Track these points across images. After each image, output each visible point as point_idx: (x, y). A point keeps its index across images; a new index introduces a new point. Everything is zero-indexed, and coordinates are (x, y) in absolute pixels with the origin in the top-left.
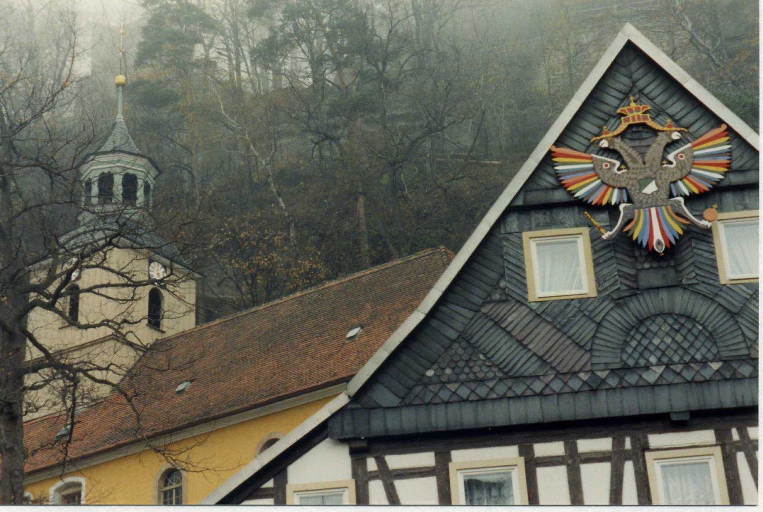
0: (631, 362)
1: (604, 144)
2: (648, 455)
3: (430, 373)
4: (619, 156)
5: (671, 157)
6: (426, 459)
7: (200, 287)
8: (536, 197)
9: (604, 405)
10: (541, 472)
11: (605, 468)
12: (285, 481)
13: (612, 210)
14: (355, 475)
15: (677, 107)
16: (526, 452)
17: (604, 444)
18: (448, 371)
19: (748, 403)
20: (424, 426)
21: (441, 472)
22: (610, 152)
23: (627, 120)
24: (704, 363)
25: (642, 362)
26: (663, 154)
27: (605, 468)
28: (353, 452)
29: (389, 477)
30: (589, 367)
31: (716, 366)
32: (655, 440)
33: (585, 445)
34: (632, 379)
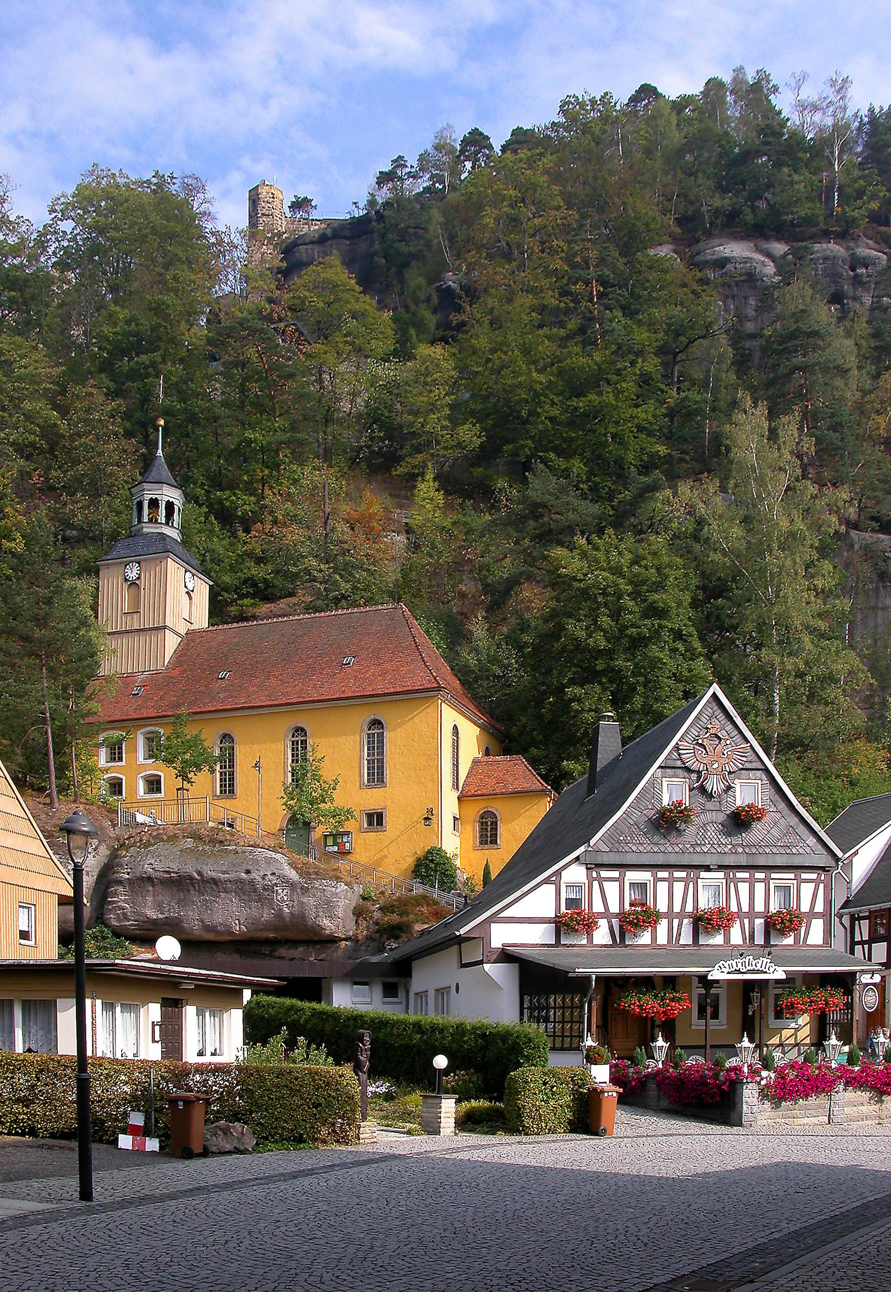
3: (621, 838)
4: (705, 749)
6: (615, 874)
7: (328, 1027)
8: (670, 763)
13: (699, 773)
15: (729, 727)
17: (683, 874)
19: (61, 907)
21: (621, 880)
28: (587, 869)
29: (601, 880)
31: (730, 847)
32: (773, 876)
33: (677, 874)
34: (698, 849)
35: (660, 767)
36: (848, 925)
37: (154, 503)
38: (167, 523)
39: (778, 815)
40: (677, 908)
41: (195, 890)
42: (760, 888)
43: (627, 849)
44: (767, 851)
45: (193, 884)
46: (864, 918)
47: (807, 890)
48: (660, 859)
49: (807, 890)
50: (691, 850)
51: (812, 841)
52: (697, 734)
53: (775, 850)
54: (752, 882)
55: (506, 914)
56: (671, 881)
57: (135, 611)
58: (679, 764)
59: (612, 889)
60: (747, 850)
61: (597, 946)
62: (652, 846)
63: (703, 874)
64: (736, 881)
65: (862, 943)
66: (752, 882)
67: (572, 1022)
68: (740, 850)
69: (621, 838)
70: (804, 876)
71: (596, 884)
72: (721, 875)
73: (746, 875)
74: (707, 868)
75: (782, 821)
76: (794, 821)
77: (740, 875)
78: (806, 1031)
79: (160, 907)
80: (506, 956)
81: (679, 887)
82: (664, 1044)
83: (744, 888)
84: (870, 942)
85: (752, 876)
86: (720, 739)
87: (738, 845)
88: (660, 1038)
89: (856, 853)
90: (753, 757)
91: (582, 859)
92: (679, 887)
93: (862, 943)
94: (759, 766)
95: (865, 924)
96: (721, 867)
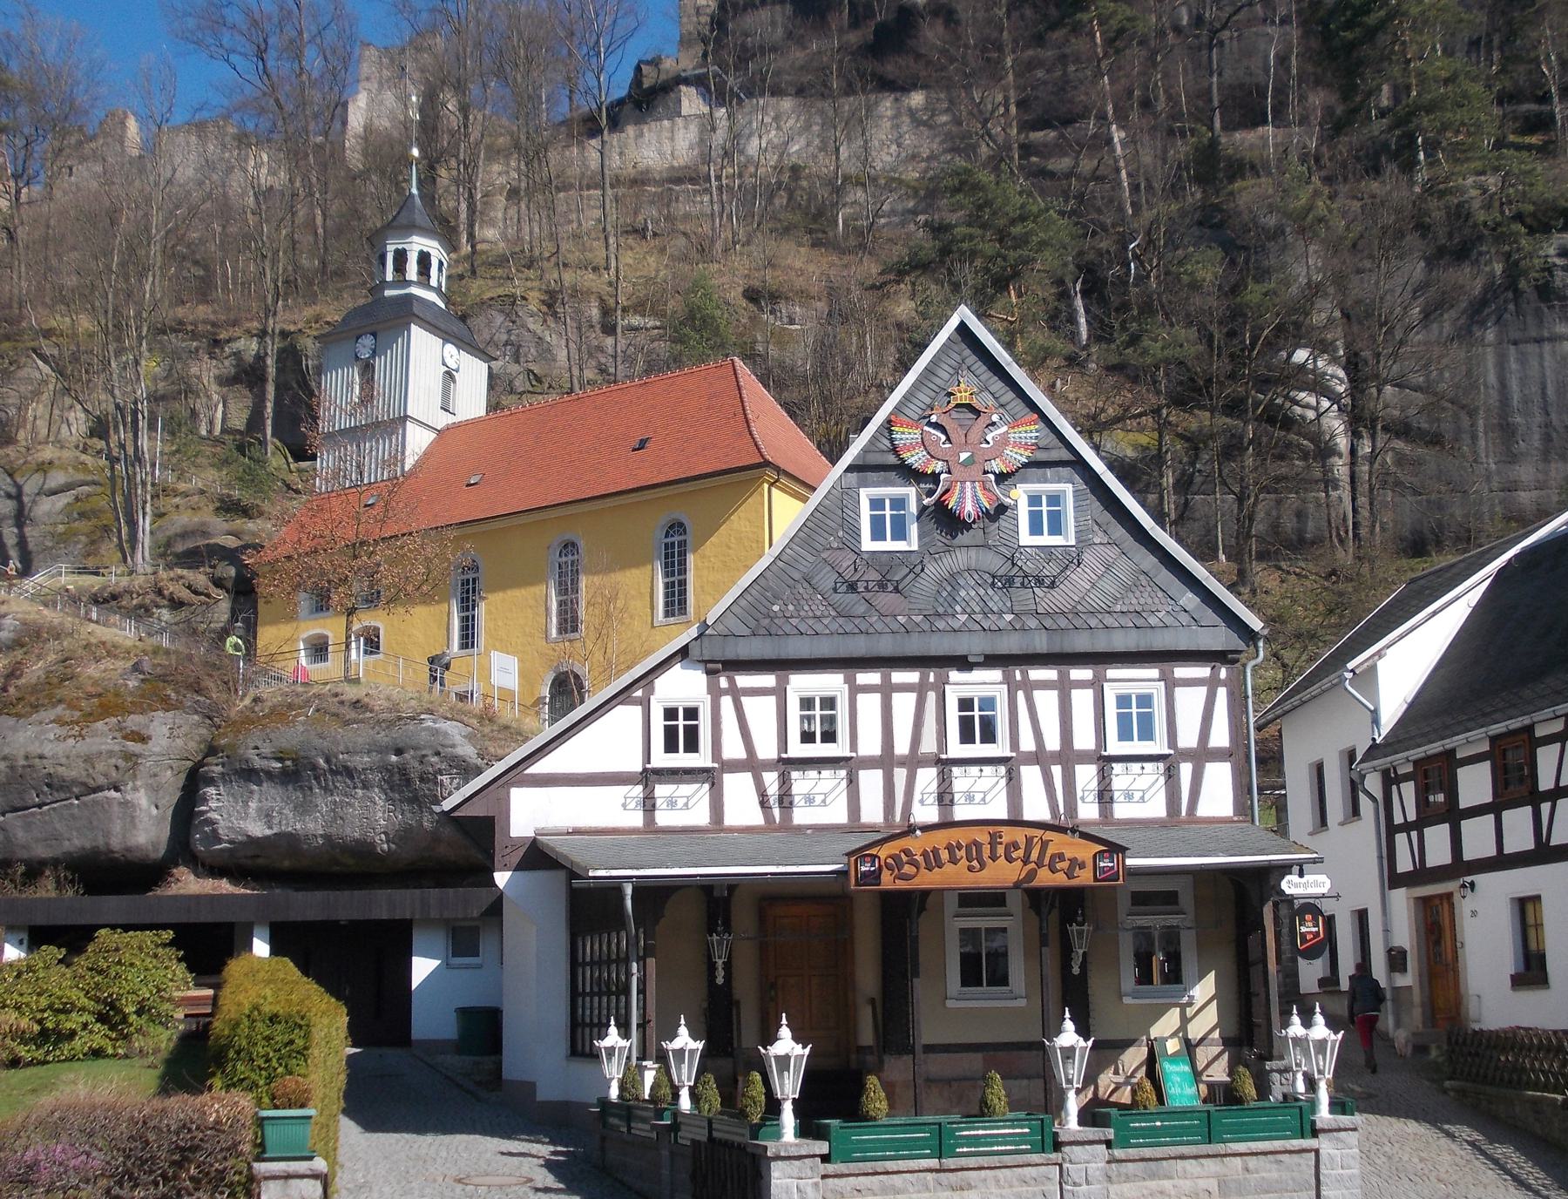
0: (941, 610)
1: (934, 419)
2: (947, 687)
3: (776, 608)
5: (989, 438)
6: (768, 680)
9: (914, 646)
10: (861, 698)
11: (911, 698)
12: (652, 691)
13: (935, 477)
14: (710, 691)
15: (997, 385)
16: (850, 681)
17: (912, 677)
18: (791, 607)
20: (843, 653)
21: (780, 693)
22: (937, 426)
23: (956, 399)
24: (1001, 613)
25: (950, 611)
26: (55, 863)
27: (911, 698)
28: (709, 673)
29: (736, 694)
30: (906, 612)
31: (1009, 617)
32: (1112, 673)
33: (899, 677)
34: (941, 624)
35: (850, 469)
36: (1379, 795)
37: (401, 257)
38: (419, 284)
39: (1112, 552)
40: (902, 747)
41: (321, 787)
42: (1082, 701)
43: (787, 628)
44: (1093, 622)
45: (317, 778)
46: (1406, 778)
47: (1190, 702)
48: (858, 647)
49: (1190, 702)
50: (926, 626)
51: (1189, 599)
52: (928, 401)
53: (1109, 620)
54: (1064, 688)
55: (541, 767)
56: (887, 691)
57: (367, 398)
58: (892, 459)
59: (761, 712)
60: (1048, 623)
61: (732, 830)
62: (841, 621)
63: (954, 675)
64: (1029, 687)
65: (1407, 827)
66: (1064, 688)
67: (600, 994)
68: (1032, 623)
69: (776, 608)
70: (1181, 672)
71: (727, 702)
72: (996, 674)
73: (1050, 674)
74: (964, 664)
75: (1123, 562)
76: (1150, 561)
77: (1036, 674)
78: (1211, 1016)
79: (267, 817)
80: (537, 856)
81: (904, 705)
82: (798, 1050)
83: (1047, 702)
84: (1420, 825)
85: (1064, 677)
86: (977, 413)
87: (1026, 613)
88: (785, 1032)
89: (1379, 654)
90: (1051, 439)
91: (695, 652)
92: (904, 705)
93: (1407, 827)
94: (1066, 455)
95: (1408, 789)
96: (991, 661)
